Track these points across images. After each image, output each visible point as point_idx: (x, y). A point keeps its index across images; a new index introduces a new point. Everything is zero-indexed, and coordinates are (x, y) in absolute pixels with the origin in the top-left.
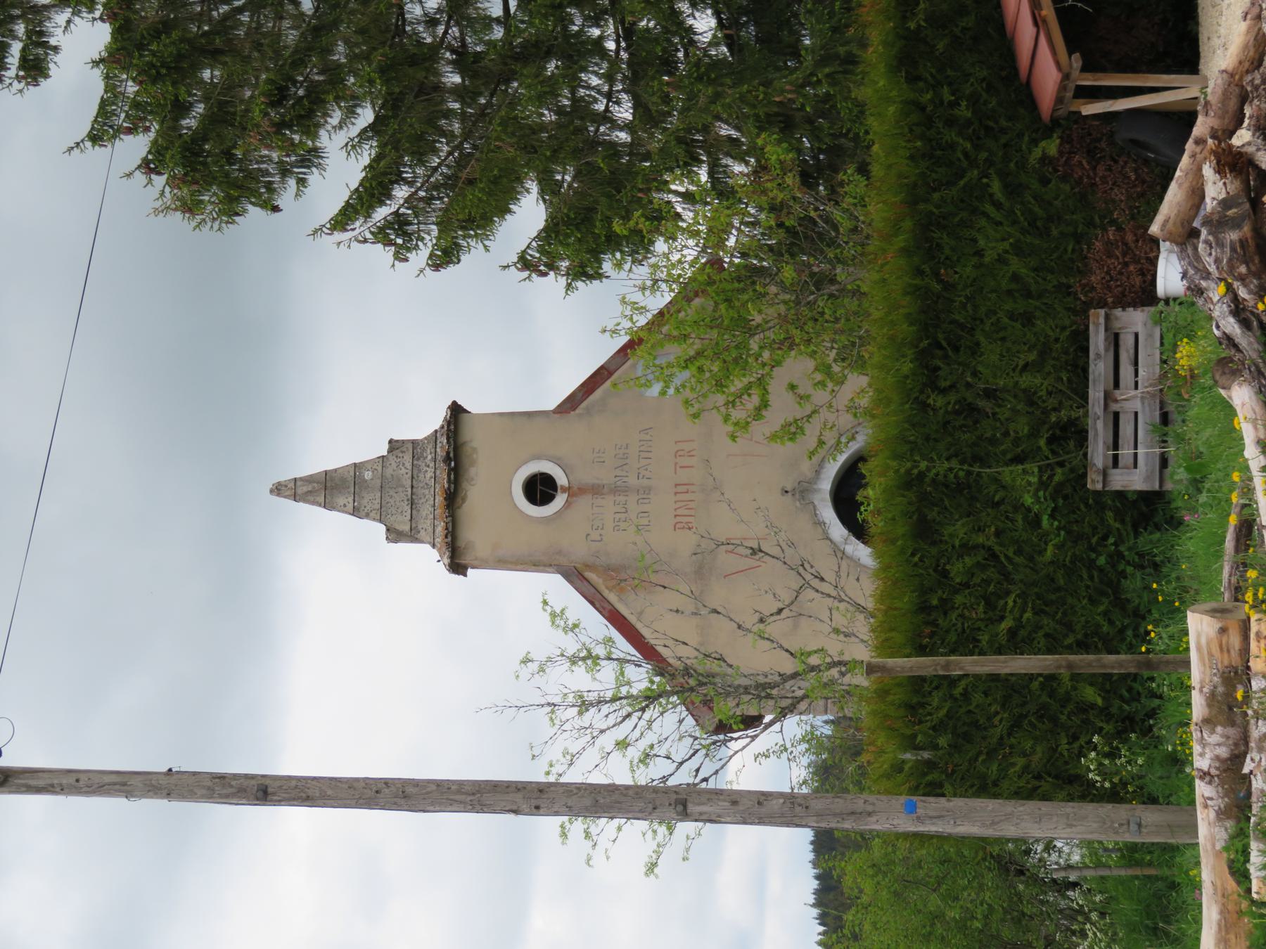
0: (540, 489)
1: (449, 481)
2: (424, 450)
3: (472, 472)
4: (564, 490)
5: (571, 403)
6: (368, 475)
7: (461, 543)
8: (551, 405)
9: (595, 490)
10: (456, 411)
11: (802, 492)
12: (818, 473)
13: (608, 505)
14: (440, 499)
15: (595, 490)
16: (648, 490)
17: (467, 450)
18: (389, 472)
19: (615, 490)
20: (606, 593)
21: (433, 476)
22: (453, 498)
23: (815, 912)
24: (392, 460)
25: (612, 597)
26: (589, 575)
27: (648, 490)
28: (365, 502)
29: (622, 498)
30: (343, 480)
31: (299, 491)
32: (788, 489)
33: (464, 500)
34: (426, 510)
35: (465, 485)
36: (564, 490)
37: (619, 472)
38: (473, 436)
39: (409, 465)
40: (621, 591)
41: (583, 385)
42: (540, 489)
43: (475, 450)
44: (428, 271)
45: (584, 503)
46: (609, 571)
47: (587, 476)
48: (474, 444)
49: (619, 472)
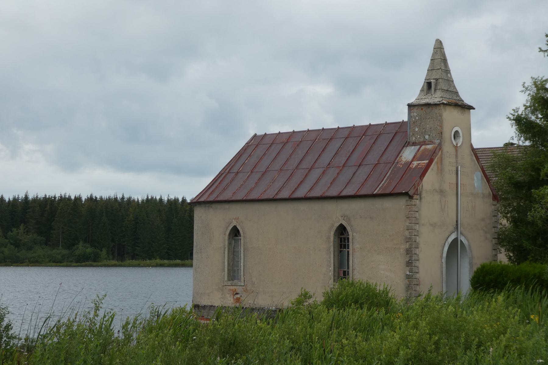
20: (436, 158)
46: (441, 159)
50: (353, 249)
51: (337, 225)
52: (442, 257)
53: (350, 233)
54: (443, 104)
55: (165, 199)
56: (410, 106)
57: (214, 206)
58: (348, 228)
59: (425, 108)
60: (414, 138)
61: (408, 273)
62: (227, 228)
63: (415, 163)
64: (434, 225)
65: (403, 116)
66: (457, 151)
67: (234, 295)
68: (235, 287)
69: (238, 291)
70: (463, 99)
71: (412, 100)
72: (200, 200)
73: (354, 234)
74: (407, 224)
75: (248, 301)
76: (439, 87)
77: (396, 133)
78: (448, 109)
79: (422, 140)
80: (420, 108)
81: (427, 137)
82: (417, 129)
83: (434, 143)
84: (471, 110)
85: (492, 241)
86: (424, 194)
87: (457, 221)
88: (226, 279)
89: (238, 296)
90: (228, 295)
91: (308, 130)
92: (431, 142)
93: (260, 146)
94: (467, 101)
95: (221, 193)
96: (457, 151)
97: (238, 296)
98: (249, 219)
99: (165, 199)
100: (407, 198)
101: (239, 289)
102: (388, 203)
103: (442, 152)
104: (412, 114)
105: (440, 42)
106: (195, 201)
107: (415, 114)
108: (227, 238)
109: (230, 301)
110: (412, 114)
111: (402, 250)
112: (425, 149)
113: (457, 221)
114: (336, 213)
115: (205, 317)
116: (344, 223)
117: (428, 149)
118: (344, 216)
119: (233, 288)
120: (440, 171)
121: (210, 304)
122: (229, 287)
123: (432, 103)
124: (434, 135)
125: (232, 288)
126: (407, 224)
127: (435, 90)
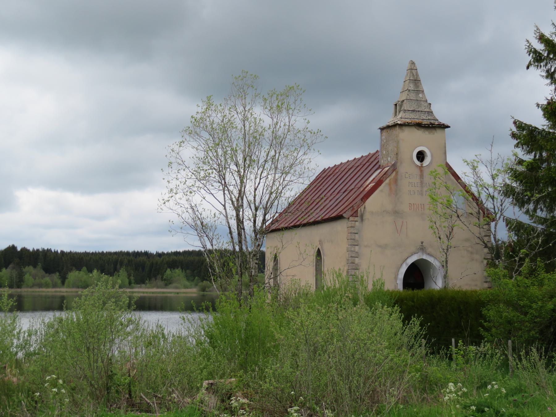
0: (421, 156)
1: (425, 124)
2: (431, 116)
3: (427, 133)
4: (422, 165)
5: (450, 169)
6: (421, 95)
7: (404, 128)
8: (448, 161)
9: (422, 176)
10: (444, 127)
11: (422, 249)
12: (429, 254)
13: (417, 180)
14: (417, 121)
15: (422, 176)
16: (422, 194)
17: (434, 131)
18: (422, 103)
19: (422, 183)
20: (388, 179)
21: (424, 119)
22: (419, 125)
23: (46, 249)
24: (426, 104)
25: (387, 181)
26: (394, 173)
27: (422, 194)
28: (412, 94)
29: (419, 185)
30: (418, 87)
31: (413, 71)
32: (423, 244)
33: (418, 129)
34: (412, 115)
35: (423, 130)
36: (422, 165)
37: (427, 184)
38: (438, 133)
39: (425, 110)
40: (389, 184)
41: (455, 172)
42: (421, 156)
43: (434, 134)
44: (513, 120)
45: (417, 171)
46: (396, 181)
47: (426, 173)
48: (435, 134)
49: (427, 184)
52: (396, 278)
54: (397, 124)
55: (143, 251)
64: (383, 247)
66: (421, 171)
70: (437, 118)
76: (402, 108)
78: (407, 130)
84: (446, 129)
85: (482, 262)
86: (367, 216)
87: (230, 228)
94: (442, 120)
96: (421, 171)
99: (143, 251)
103: (397, 173)
105: (413, 63)
113: (230, 228)
115: (333, 395)
120: (395, 191)
127: (400, 112)
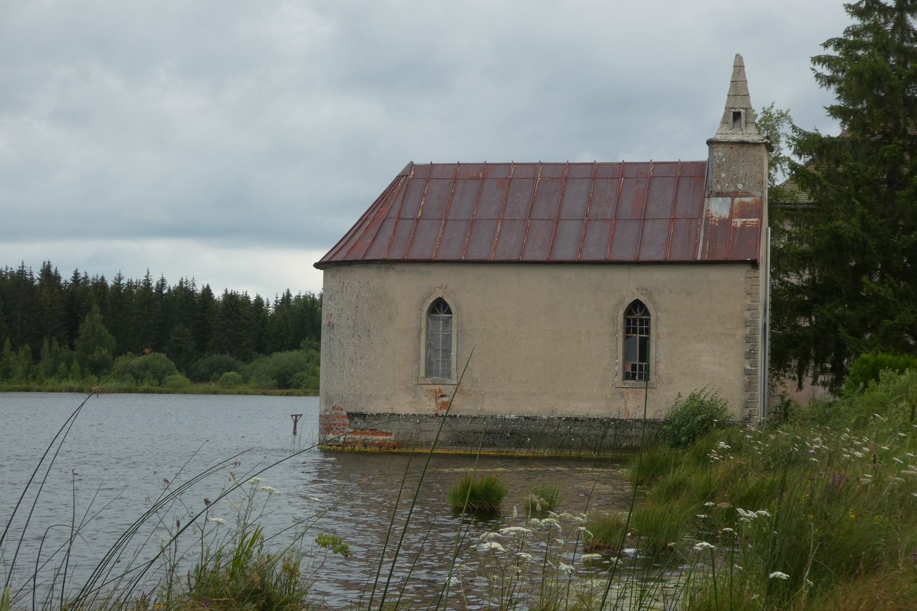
50: (658, 335)
51: (629, 300)
53: (652, 312)
56: (710, 143)
57: (398, 267)
58: (649, 306)
59: (736, 148)
60: (719, 187)
61: (748, 367)
62: (424, 301)
63: (739, 222)
65: (701, 154)
67: (436, 398)
68: (440, 387)
69: (445, 392)
71: (712, 136)
72: (333, 259)
73: (659, 314)
74: (748, 302)
75: (463, 406)
77: (691, 177)
79: (732, 189)
80: (729, 146)
81: (740, 186)
82: (723, 175)
83: (753, 196)
88: (423, 374)
89: (445, 399)
90: (426, 399)
91: (459, 164)
92: (747, 194)
93: (414, 181)
95: (349, 252)
97: (445, 399)
98: (464, 289)
100: (749, 268)
101: (448, 390)
102: (716, 274)
104: (716, 154)
106: (325, 260)
107: (721, 154)
108: (424, 315)
109: (429, 406)
110: (716, 154)
111: (738, 337)
112: (742, 203)
114: (628, 285)
116: (642, 299)
117: (748, 203)
118: (641, 289)
119: (437, 387)
121: (390, 411)
122: (428, 387)
123: (751, 141)
124: (751, 185)
125: (432, 387)
126: (748, 302)
